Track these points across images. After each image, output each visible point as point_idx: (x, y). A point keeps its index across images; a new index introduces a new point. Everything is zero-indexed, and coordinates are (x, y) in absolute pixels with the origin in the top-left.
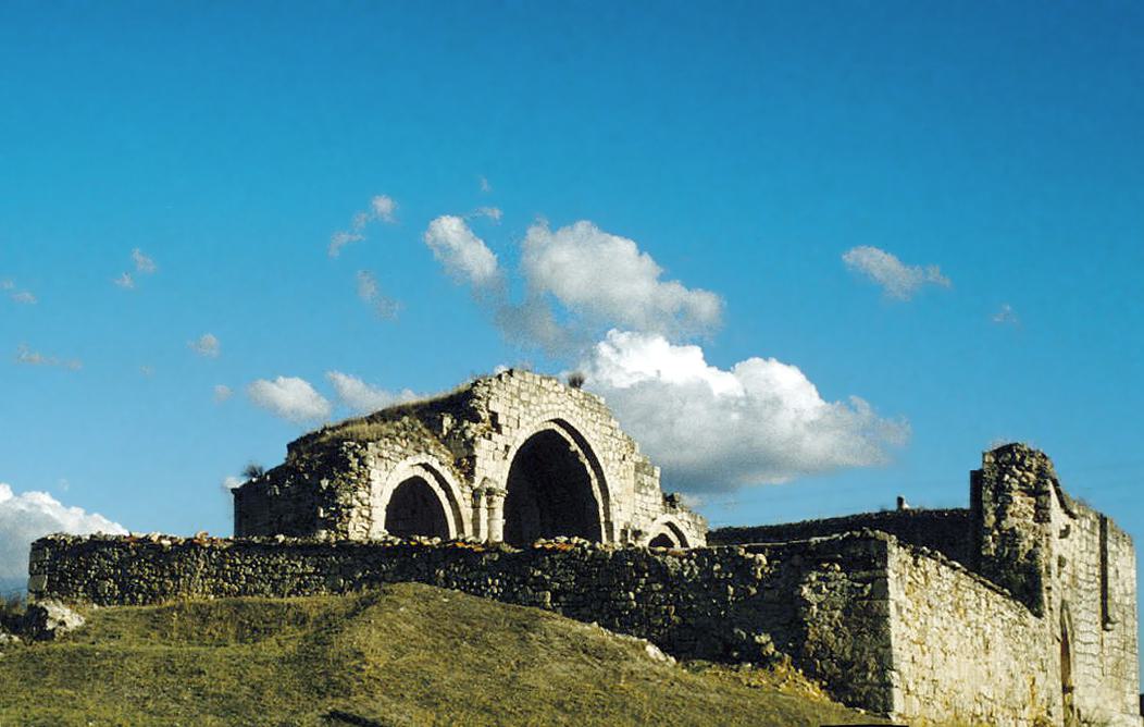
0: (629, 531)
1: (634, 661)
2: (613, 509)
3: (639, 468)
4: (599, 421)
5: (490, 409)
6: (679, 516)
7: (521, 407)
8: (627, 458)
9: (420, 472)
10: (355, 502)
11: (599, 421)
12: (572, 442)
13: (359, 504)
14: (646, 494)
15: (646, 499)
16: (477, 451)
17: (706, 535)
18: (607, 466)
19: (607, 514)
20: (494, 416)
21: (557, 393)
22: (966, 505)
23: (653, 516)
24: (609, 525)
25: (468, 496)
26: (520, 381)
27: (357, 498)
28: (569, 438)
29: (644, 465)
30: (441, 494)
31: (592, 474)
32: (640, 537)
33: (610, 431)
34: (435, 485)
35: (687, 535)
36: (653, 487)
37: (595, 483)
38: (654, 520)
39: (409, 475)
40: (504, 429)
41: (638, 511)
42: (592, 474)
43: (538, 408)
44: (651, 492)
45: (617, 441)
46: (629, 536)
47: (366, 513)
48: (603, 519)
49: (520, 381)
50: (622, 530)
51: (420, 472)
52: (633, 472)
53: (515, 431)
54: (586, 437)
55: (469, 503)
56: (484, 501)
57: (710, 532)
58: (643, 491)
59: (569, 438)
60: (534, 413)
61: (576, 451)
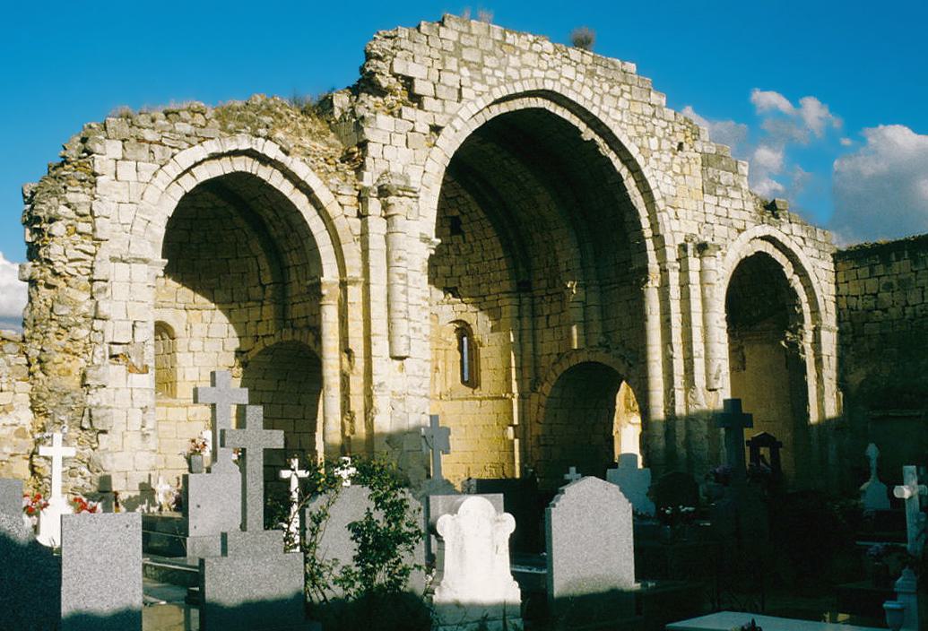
0: (690, 246)
1: (664, 473)
2: (664, 218)
3: (707, 161)
4: (627, 96)
5: (396, 70)
6: (786, 229)
7: (464, 71)
8: (686, 147)
9: (768, 248)
10: (63, 209)
11: (627, 96)
12: (582, 126)
13: (71, 214)
14: (726, 196)
15: (725, 203)
16: (368, 133)
17: (833, 255)
18: (646, 158)
19: (654, 225)
20: (408, 82)
21: (539, 54)
22: (282, 447)
23: (740, 225)
24: (659, 238)
25: (349, 197)
26: (461, 33)
27: (68, 205)
28: (575, 121)
29: (720, 157)
30: (300, 200)
31: (624, 172)
32: (707, 252)
33: (649, 111)
34: (286, 188)
35: (802, 256)
36: (736, 187)
37: (630, 184)
38: (739, 231)
39: (750, 251)
40: (428, 102)
41: (711, 219)
42: (624, 172)
43: (498, 73)
44: (733, 194)
45: (665, 124)
46: (690, 252)
47: (84, 227)
48: (648, 233)
49: (461, 33)
50: (680, 246)
51: (768, 248)
52: (699, 167)
53: (452, 107)
54: (603, 118)
55: (353, 211)
56: (374, 206)
57: (839, 251)
58: (720, 192)
59: (575, 121)
60: (491, 81)
61: (593, 140)
